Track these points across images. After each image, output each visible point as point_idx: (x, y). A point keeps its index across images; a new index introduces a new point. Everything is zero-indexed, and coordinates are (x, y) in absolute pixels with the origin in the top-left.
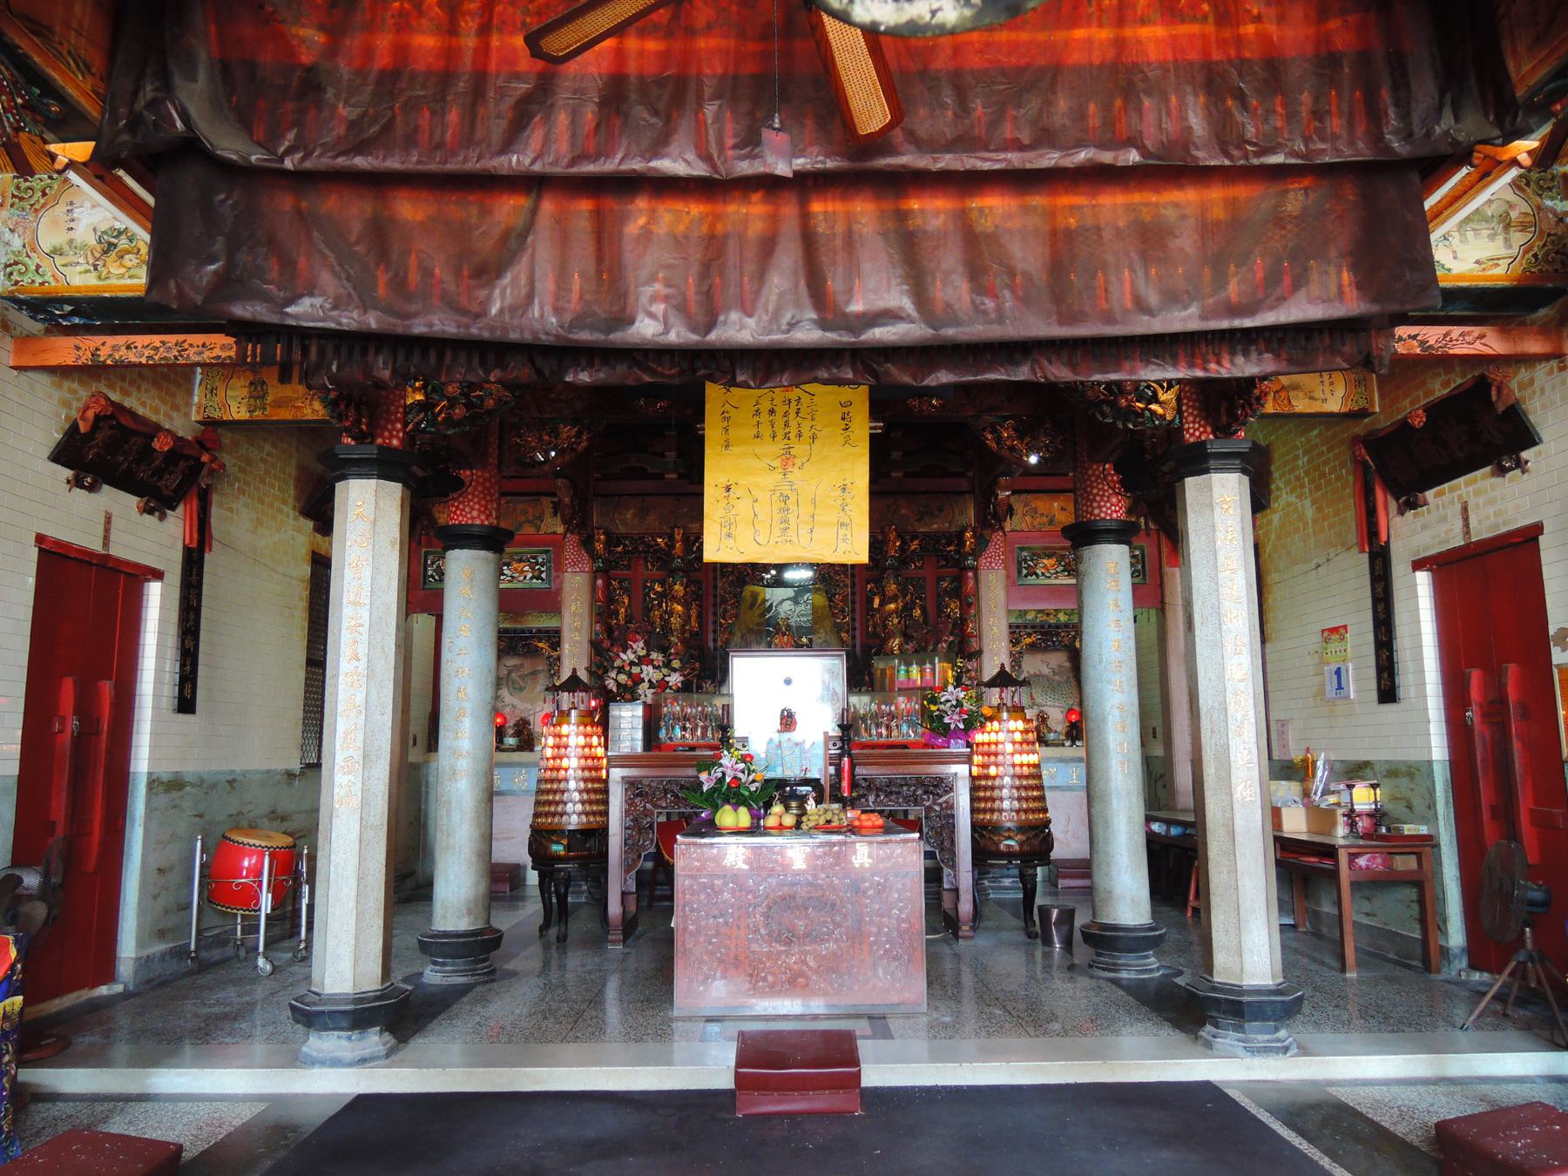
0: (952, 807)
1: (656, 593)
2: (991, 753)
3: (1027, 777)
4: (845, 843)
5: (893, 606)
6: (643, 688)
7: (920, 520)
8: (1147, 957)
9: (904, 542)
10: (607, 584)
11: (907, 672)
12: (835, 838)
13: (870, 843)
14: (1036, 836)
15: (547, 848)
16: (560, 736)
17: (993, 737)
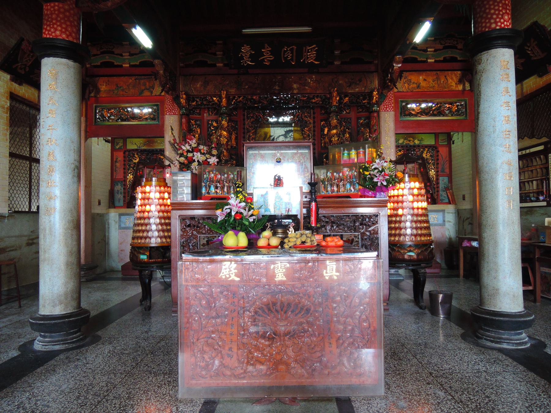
0: (377, 233)
1: (214, 127)
2: (398, 201)
3: (421, 215)
4: (317, 260)
5: (335, 131)
6: (194, 165)
7: (349, 86)
8: (521, 333)
9: (341, 98)
10: (188, 122)
11: (349, 154)
12: (309, 256)
13: (337, 260)
14: (426, 250)
15: (138, 257)
16: (145, 193)
17: (400, 192)
